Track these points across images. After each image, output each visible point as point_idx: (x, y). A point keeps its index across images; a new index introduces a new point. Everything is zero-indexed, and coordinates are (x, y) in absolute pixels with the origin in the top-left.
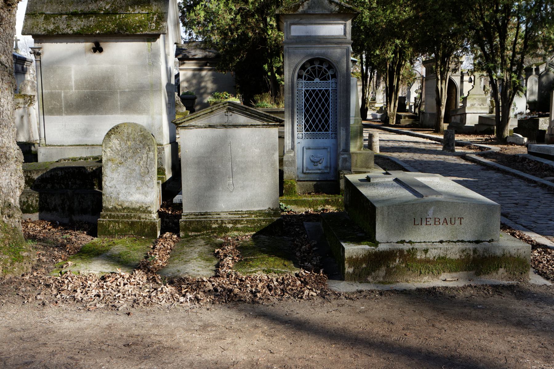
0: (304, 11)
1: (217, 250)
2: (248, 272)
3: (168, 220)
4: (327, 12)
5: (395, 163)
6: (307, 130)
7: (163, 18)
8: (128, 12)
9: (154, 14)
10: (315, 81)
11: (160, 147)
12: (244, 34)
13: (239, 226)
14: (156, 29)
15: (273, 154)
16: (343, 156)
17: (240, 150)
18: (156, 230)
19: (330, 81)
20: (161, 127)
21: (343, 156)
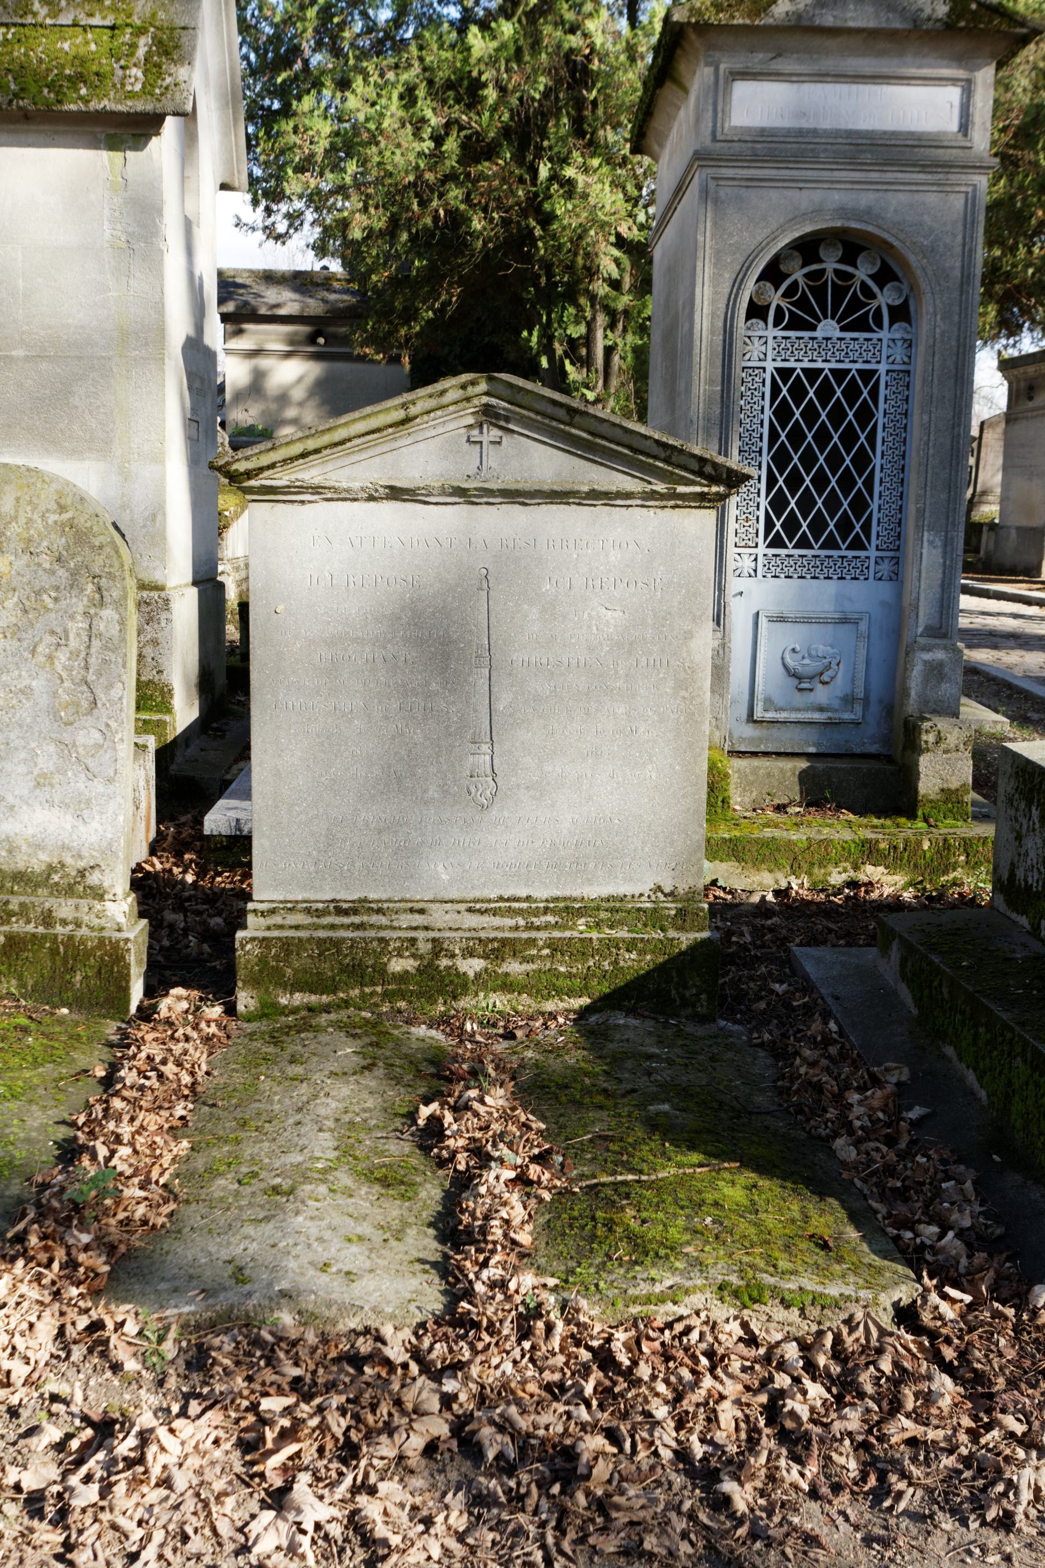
0: (799, 16)
1: (425, 1111)
2: (635, 1300)
3: (177, 918)
4: (897, 25)
5: (1009, 686)
6: (776, 543)
7: (177, 47)
8: (29, 20)
9: (140, 31)
10: (819, 333)
11: (155, 594)
12: (457, 219)
13: (514, 968)
14: (147, 90)
15: (689, 635)
16: (927, 656)
17: (534, 613)
18: (127, 978)
19: (884, 334)
20: (156, 514)
21: (927, 656)
